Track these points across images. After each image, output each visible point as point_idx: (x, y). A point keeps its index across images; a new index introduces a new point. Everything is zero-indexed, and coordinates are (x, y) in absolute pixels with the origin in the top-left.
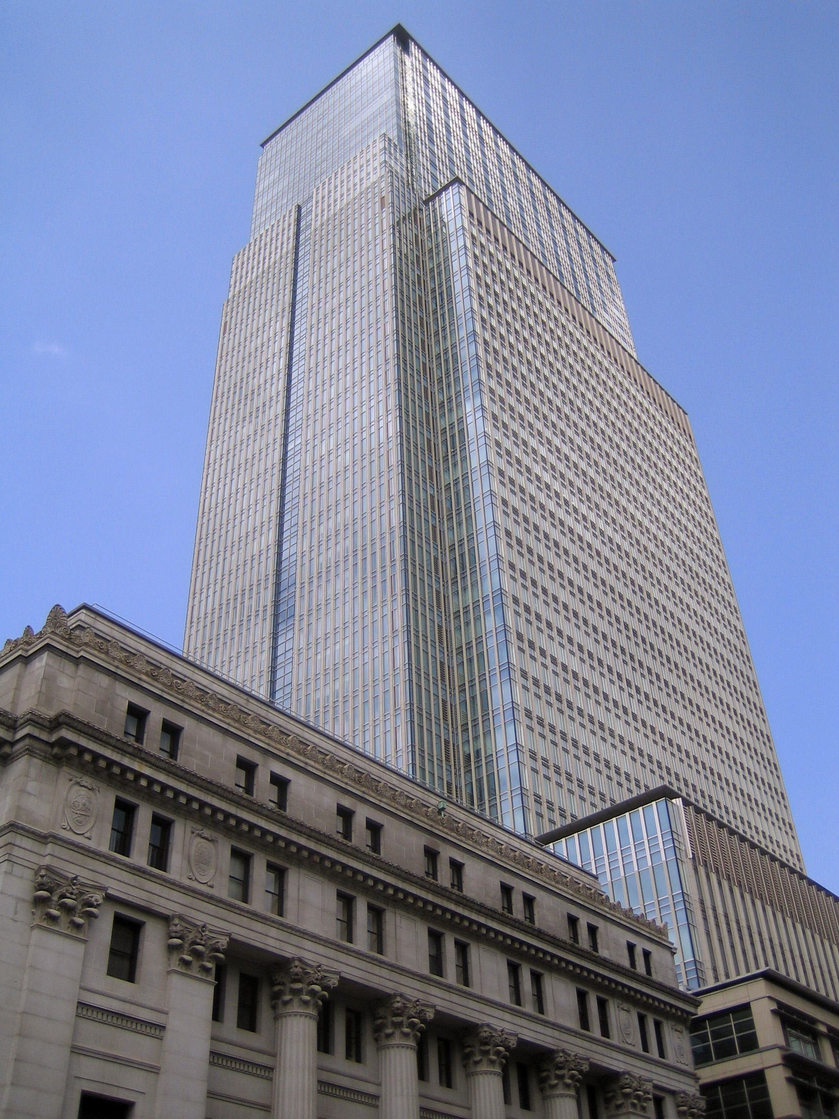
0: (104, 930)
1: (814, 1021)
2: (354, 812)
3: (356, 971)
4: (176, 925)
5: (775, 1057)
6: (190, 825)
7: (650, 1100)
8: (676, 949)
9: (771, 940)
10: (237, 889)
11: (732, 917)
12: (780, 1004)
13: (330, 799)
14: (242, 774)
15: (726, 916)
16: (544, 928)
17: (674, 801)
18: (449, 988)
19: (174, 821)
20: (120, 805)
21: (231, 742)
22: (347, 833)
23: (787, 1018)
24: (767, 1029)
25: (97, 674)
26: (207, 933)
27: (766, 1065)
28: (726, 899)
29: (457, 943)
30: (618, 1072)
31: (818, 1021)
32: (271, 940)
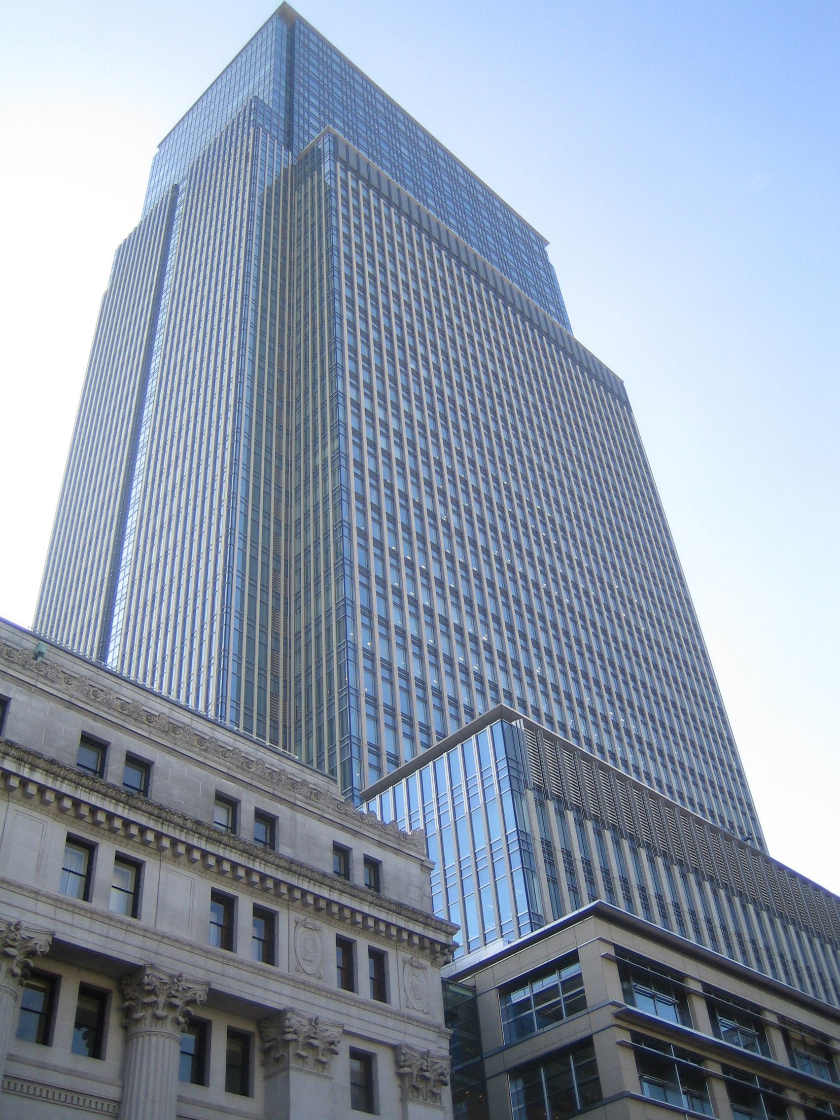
0: (342, 1067)
1: (682, 977)
2: (240, 801)
3: (84, 935)
4: (148, 976)
5: (605, 1017)
6: (294, 915)
7: (445, 1084)
8: (434, 864)
9: (808, 969)
10: (75, 883)
11: (732, 929)
12: (618, 949)
13: (70, 727)
14: (262, 827)
15: (821, 974)
16: (14, 739)
17: (514, 723)
18: (361, 1004)
19: (144, 862)
20: (217, 897)
21: (73, 714)
22: (234, 826)
23: (632, 970)
24: (603, 984)
25: (308, 818)
26: (183, 983)
27: (595, 1030)
28: (565, 832)
29: (259, 912)
30: (280, 1011)
31: (688, 976)
32: (126, 948)
